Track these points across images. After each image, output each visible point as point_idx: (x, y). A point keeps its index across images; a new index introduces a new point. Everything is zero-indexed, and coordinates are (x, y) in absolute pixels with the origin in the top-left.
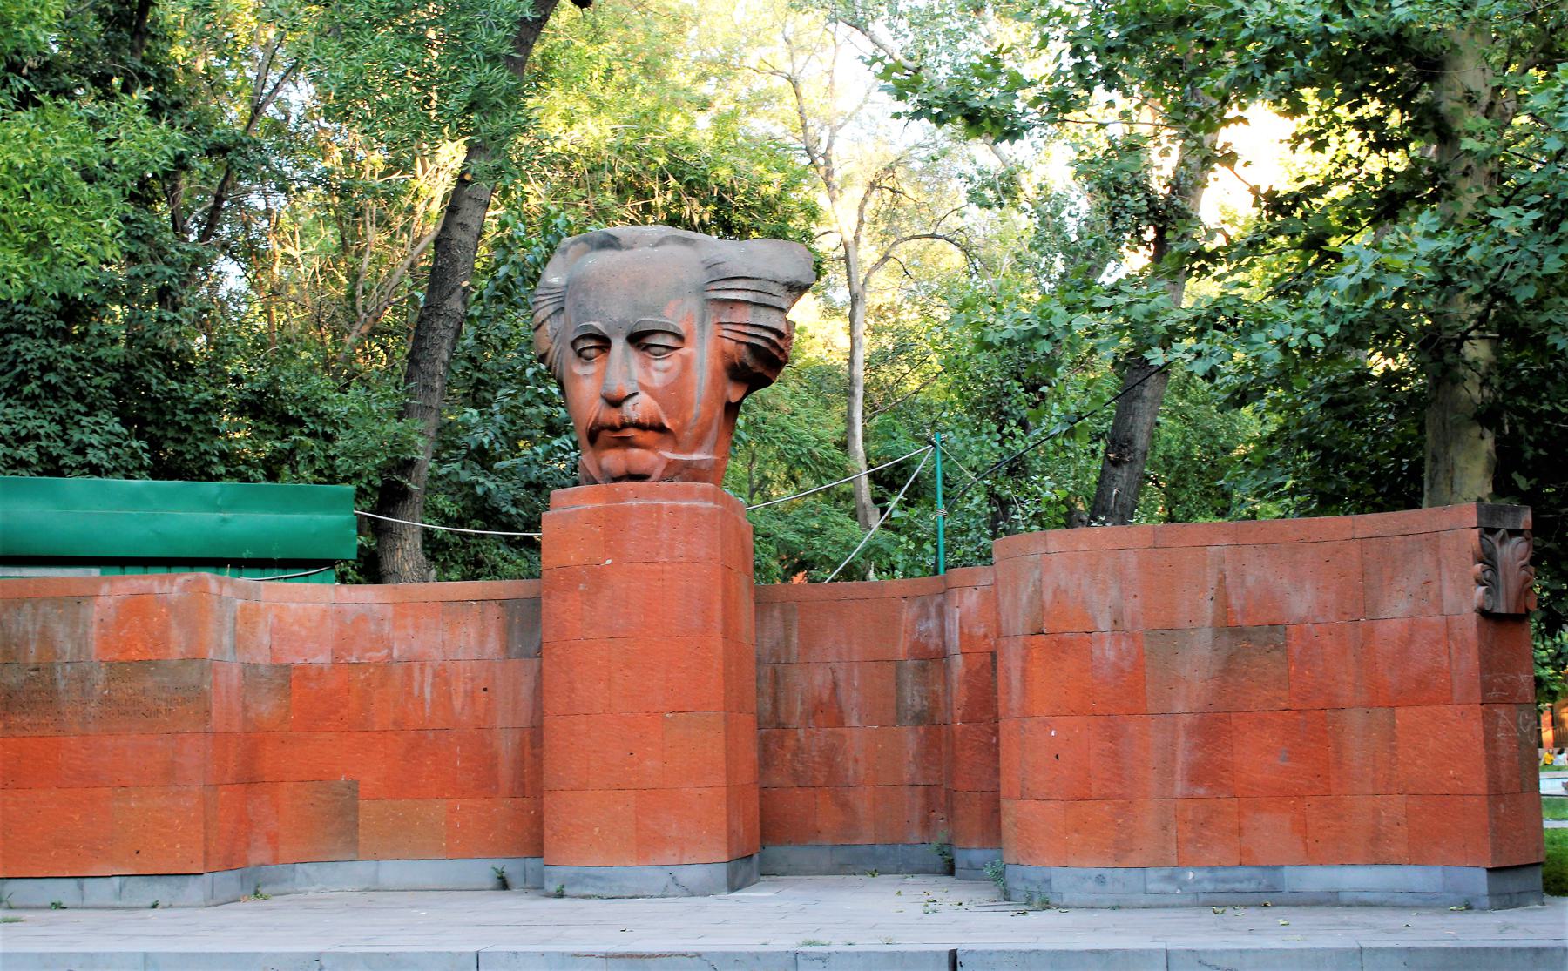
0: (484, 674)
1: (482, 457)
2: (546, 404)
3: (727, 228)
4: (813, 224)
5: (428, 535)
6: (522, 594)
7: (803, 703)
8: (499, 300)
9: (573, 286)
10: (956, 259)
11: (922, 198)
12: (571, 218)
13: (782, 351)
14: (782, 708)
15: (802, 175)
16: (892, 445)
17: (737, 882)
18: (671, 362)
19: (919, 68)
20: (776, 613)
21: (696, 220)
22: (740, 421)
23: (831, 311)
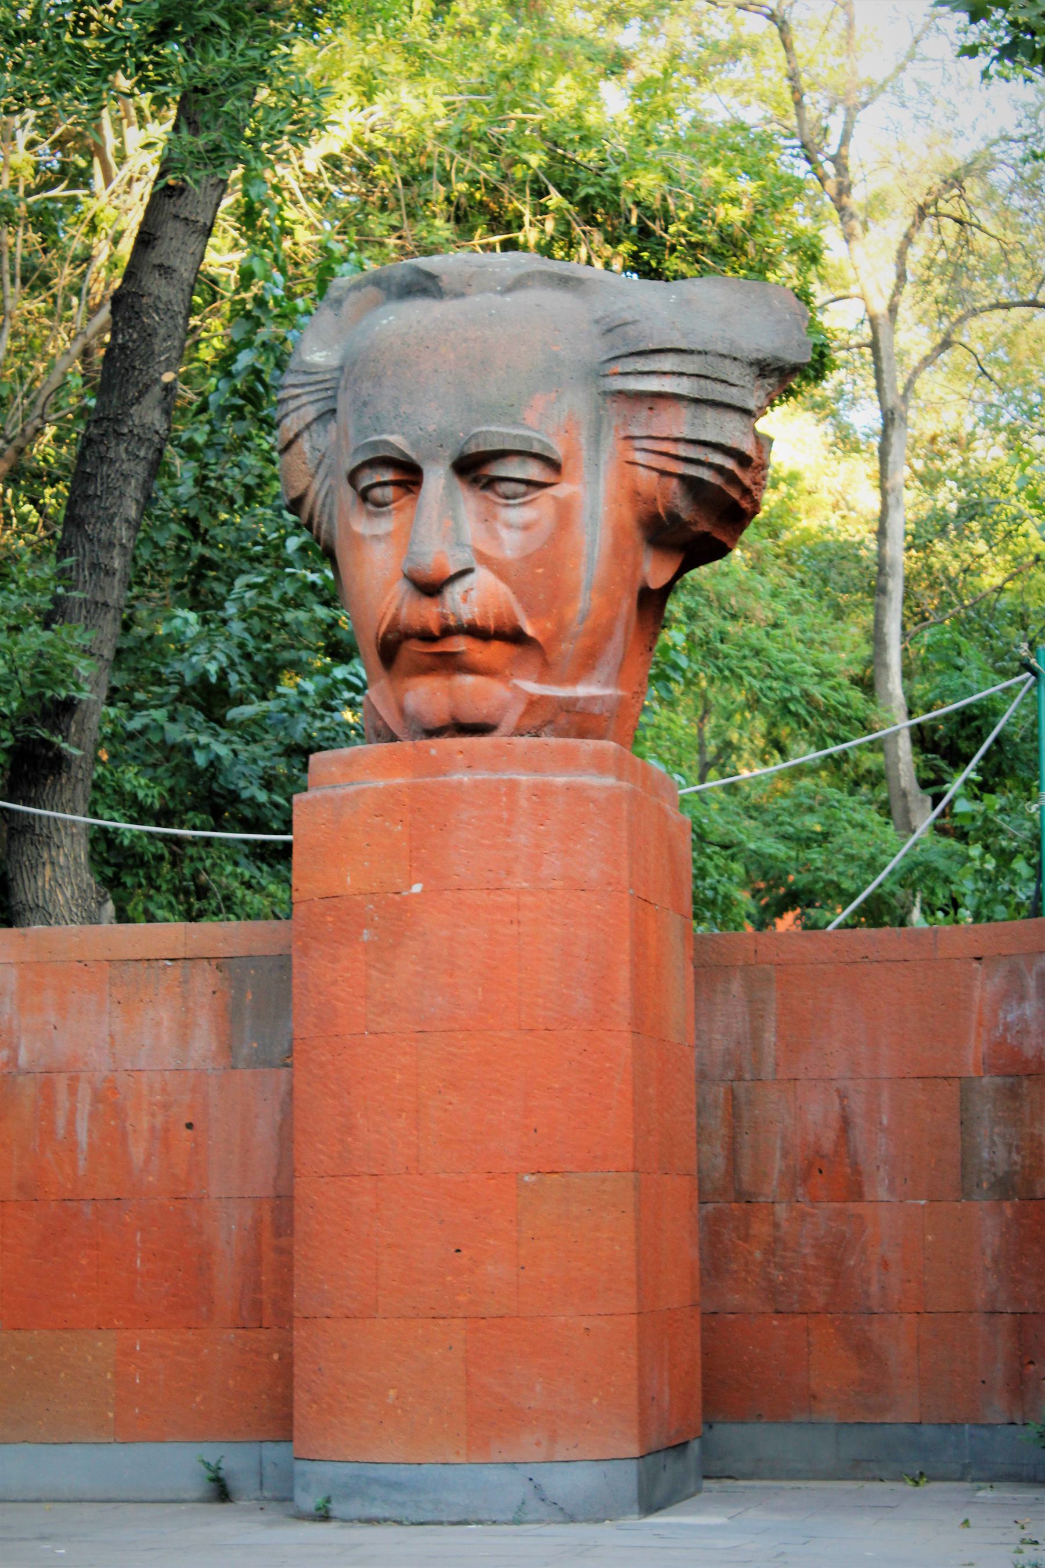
1: (210, 699)
2: (326, 603)
5: (103, 842)
7: (785, 1154)
8: (239, 414)
13: (746, 492)
14: (746, 1163)
20: (736, 987)
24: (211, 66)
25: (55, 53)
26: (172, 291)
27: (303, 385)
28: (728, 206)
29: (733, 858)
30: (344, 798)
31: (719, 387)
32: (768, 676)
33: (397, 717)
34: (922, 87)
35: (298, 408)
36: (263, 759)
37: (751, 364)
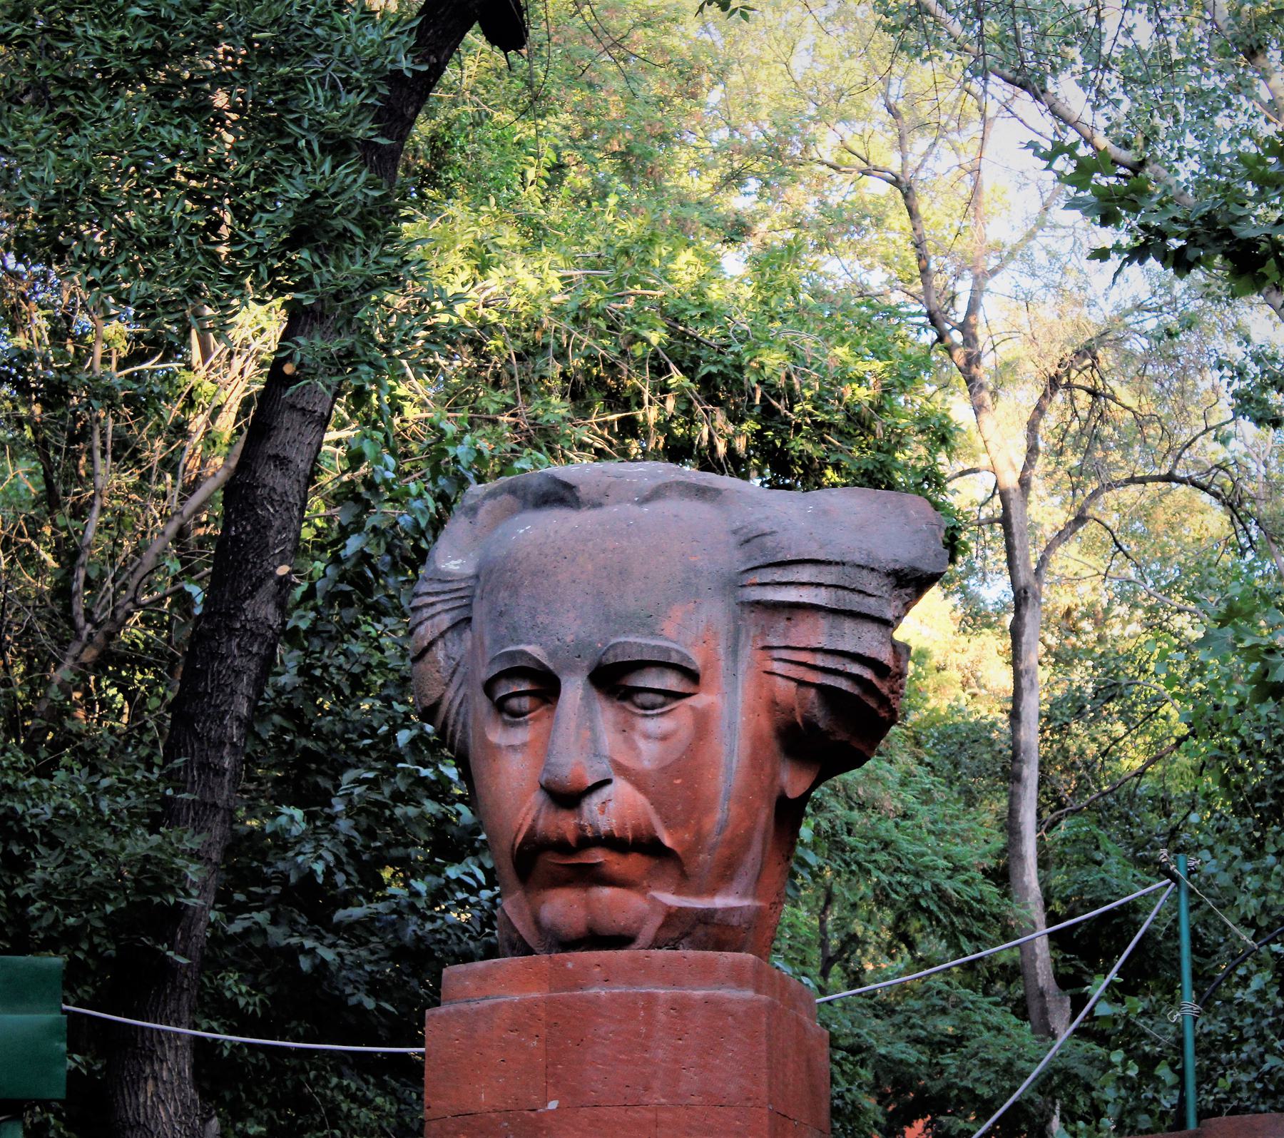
1: (312, 900)
2: (433, 797)
3: (783, 468)
4: (942, 457)
8: (346, 600)
9: (488, 576)
10: (1215, 520)
11: (1148, 407)
12: (484, 445)
13: (884, 701)
15: (923, 363)
16: (1093, 876)
18: (674, 722)
19: (1143, 163)
21: (721, 449)
22: (806, 833)
23: (975, 619)
24: (345, 274)
25: (186, 260)
26: (288, 483)
27: (437, 594)
28: (855, 386)
29: (863, 1063)
30: (477, 1013)
31: (857, 598)
32: (897, 870)
33: (533, 928)
34: (1053, 256)
35: (433, 616)
36: (370, 962)
37: (888, 575)
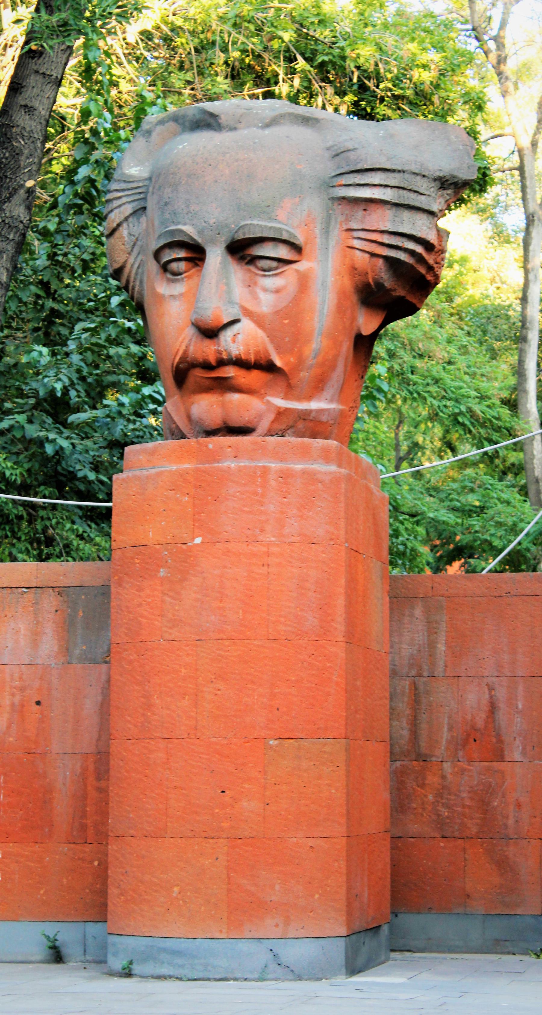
0: (37, 684)
6: (88, 580)
7: (450, 729)
13: (430, 268)
14: (424, 734)
17: (361, 960)
20: (418, 612)
23: (500, 236)
26: (33, 124)
27: (123, 190)
28: (421, 70)
29: (418, 523)
30: (148, 477)
31: (412, 195)
32: (444, 397)
35: (120, 206)
37: (435, 180)
